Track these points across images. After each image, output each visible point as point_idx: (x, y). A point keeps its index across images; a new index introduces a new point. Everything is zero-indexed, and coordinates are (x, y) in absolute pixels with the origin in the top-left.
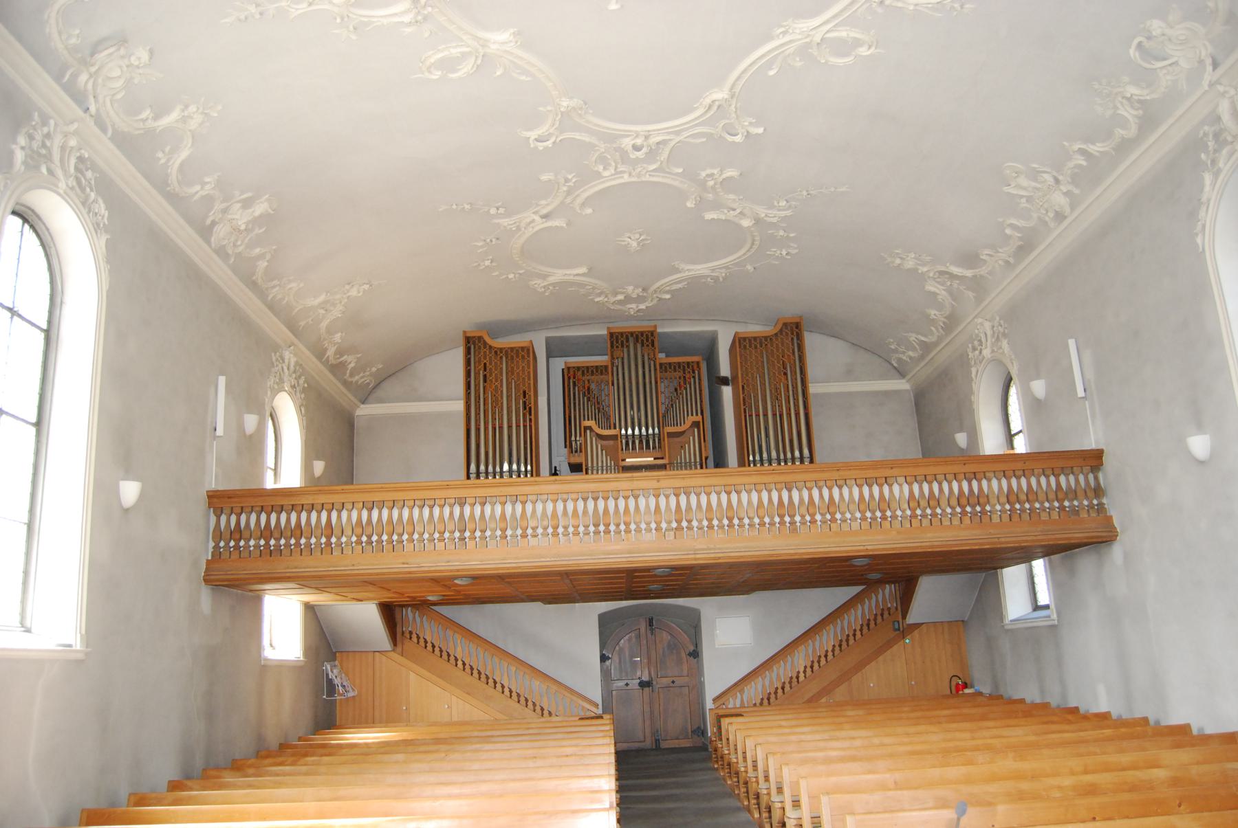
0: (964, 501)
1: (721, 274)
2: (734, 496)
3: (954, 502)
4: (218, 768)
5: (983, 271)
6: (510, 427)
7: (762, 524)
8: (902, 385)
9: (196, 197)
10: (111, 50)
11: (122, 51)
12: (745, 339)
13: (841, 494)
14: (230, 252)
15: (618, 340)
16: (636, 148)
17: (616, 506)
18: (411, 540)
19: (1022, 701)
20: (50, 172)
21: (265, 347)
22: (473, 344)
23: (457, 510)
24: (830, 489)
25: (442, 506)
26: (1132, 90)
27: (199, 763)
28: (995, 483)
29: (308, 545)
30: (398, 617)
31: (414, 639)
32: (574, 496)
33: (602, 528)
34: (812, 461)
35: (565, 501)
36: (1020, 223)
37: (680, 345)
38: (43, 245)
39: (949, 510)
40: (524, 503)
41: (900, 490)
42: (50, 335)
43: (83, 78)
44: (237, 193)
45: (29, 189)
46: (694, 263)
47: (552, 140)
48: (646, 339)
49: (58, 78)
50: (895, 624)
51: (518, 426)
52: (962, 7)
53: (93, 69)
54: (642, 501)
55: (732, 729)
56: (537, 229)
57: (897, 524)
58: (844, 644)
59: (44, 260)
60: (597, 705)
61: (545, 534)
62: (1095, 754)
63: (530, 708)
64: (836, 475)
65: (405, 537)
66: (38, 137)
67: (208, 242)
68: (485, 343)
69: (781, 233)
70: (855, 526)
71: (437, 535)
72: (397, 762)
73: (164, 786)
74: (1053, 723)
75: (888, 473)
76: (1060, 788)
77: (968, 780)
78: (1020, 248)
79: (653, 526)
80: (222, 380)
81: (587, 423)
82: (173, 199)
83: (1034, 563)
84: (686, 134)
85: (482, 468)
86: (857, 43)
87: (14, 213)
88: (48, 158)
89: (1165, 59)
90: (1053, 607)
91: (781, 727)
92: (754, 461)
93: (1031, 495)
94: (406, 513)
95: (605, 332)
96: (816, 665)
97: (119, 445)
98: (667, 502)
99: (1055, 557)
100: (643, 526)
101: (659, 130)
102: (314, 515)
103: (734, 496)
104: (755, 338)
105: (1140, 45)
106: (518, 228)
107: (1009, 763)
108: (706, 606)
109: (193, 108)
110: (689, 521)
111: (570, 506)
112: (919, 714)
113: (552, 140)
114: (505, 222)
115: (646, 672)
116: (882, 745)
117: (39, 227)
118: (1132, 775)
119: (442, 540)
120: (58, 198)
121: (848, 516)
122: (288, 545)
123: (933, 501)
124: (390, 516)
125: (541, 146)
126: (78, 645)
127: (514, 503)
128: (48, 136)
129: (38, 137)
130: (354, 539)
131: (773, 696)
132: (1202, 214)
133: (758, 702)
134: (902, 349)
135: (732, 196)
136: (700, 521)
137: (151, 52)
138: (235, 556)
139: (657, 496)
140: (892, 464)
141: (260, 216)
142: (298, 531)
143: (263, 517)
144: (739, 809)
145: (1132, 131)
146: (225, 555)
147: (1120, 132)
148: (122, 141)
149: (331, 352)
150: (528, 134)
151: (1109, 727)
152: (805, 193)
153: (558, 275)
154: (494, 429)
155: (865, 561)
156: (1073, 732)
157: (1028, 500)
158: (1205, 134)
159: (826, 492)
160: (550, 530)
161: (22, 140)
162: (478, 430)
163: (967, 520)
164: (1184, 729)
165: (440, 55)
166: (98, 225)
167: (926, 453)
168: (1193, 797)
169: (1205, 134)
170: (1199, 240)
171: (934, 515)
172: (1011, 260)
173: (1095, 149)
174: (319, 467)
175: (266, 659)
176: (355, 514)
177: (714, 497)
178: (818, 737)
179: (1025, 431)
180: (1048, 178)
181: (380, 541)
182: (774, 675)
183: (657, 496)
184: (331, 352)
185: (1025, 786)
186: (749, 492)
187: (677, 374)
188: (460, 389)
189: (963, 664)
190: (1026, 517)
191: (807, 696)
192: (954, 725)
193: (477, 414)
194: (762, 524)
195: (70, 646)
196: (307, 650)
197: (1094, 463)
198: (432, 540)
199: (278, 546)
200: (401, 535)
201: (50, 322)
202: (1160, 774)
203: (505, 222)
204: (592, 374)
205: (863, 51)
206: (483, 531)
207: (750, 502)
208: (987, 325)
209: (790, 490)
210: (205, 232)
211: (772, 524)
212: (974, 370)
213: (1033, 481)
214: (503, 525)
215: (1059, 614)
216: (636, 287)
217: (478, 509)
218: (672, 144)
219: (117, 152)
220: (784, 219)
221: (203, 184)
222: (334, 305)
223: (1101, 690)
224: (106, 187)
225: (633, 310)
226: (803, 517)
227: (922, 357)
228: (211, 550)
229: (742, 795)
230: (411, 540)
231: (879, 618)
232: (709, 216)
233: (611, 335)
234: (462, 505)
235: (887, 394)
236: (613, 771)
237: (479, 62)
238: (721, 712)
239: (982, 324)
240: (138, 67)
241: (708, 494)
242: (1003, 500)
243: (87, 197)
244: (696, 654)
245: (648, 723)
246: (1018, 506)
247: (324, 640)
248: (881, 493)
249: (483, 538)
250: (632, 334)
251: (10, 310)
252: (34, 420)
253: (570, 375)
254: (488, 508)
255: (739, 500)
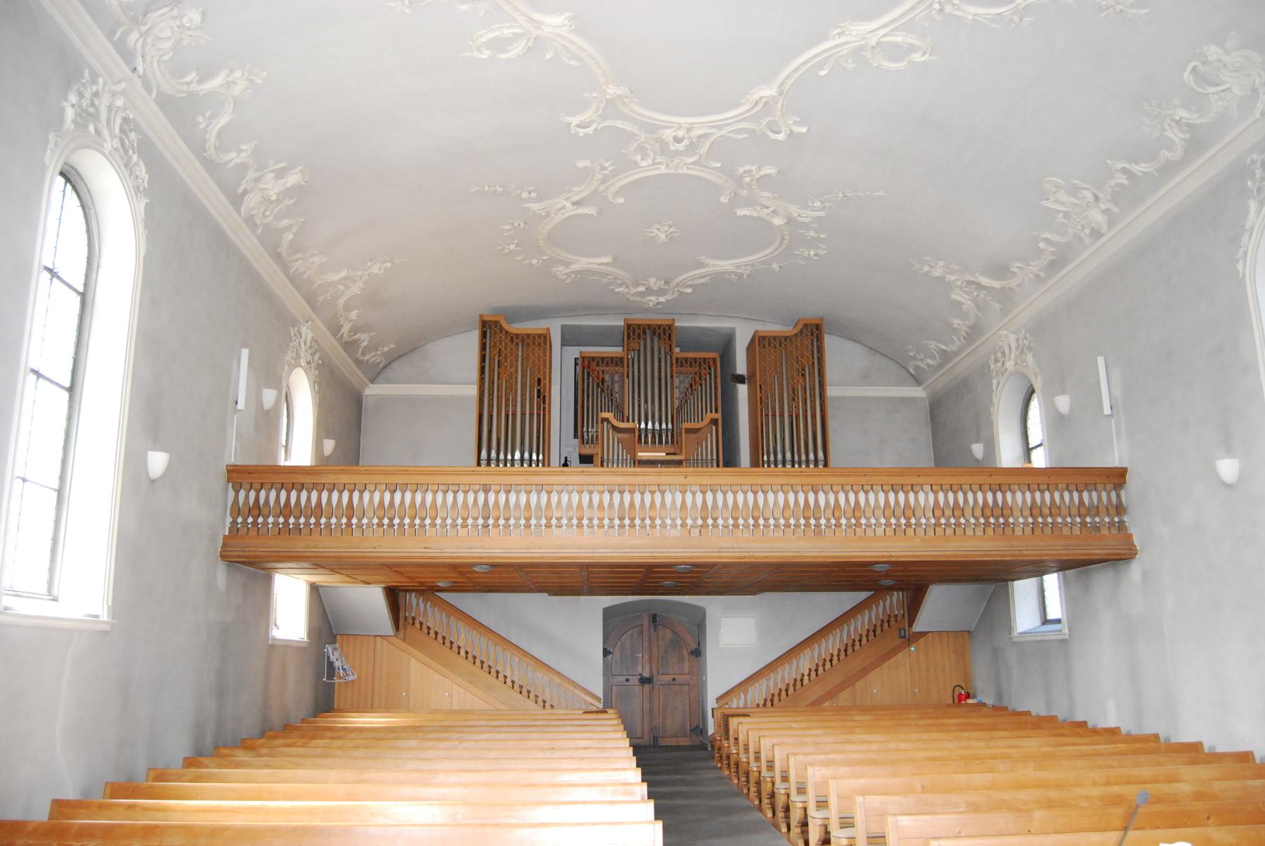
0: (988, 512)
1: (746, 271)
2: (761, 496)
3: (978, 513)
4: (225, 746)
5: (1012, 283)
6: (523, 414)
7: (787, 525)
8: (918, 392)
9: (231, 165)
10: (165, 10)
11: (175, 12)
12: (764, 338)
13: (867, 499)
14: (258, 222)
15: (634, 332)
16: (677, 140)
17: (642, 500)
18: (433, 525)
19: (1027, 713)
20: (97, 131)
21: (284, 321)
22: (489, 329)
23: (481, 496)
24: (856, 493)
25: (466, 492)
26: (1181, 113)
27: (209, 740)
28: (1019, 495)
29: (328, 525)
30: (401, 602)
31: (417, 625)
32: (600, 488)
33: (627, 522)
34: (826, 465)
35: (591, 493)
36: (1055, 238)
37: (698, 340)
38: (83, 206)
39: (973, 521)
40: (549, 493)
41: (925, 498)
42: (85, 299)
43: (134, 36)
44: (271, 162)
45: (76, 149)
46: (719, 258)
47: (593, 127)
48: (664, 332)
49: (110, 35)
50: (900, 632)
51: (531, 414)
52: (1021, 19)
53: (144, 29)
54: (668, 497)
55: (743, 730)
56: (566, 215)
57: (920, 532)
58: (850, 649)
59: (83, 221)
60: (598, 699)
61: (570, 525)
62: (1113, 767)
63: (534, 704)
64: (863, 480)
65: (428, 521)
66: (88, 94)
67: (239, 213)
68: (501, 329)
69: (812, 233)
70: (880, 531)
71: (460, 521)
72: (412, 749)
73: (179, 762)
74: (1063, 735)
75: (915, 480)
76: (1087, 797)
77: (993, 786)
78: (1052, 263)
79: (679, 522)
80: (245, 353)
81: (605, 415)
82: (211, 166)
83: (1046, 577)
84: (729, 129)
85: (493, 454)
86: (912, 49)
87: (62, 174)
88: (96, 117)
89: (1218, 85)
90: (1064, 621)
91: (790, 728)
92: (769, 462)
93: (1054, 509)
94: (429, 497)
95: (622, 323)
96: (821, 669)
97: (150, 416)
98: (694, 499)
99: (1070, 572)
100: (668, 521)
101: (701, 124)
102: (335, 495)
103: (761, 496)
104: (775, 338)
105: (1194, 69)
106: (548, 214)
107: (1028, 773)
108: (712, 605)
109: (238, 74)
110: (715, 519)
111: (596, 498)
112: (928, 722)
113: (593, 127)
114: (536, 207)
115: (647, 669)
116: (898, 750)
117: (81, 187)
118: (1154, 788)
119: (464, 526)
120: (103, 159)
121: (873, 521)
122: (307, 524)
123: (957, 510)
124: (413, 501)
125: (582, 132)
126: (104, 617)
127: (539, 492)
128: (96, 94)
129: (88, 94)
130: (375, 521)
131: (776, 698)
132: (1245, 239)
133: (762, 703)
134: (921, 356)
135: (766, 194)
136: (725, 520)
137: (203, 14)
138: (253, 533)
139: (683, 492)
140: (918, 472)
141: (293, 187)
142: (318, 510)
143: (283, 494)
144: (749, 809)
145: (1178, 153)
146: (243, 532)
147: (1165, 154)
148: (167, 103)
149: (346, 329)
150: (569, 119)
151: (1120, 742)
152: (841, 195)
153: (582, 263)
154: (507, 416)
155: (886, 567)
156: (1089, 744)
157: (1051, 515)
158: (1253, 162)
159: (852, 496)
160: (575, 521)
161: (73, 98)
162: (491, 416)
163: (990, 531)
164: (1195, 747)
165: (491, 35)
166: (138, 188)
167: (937, 465)
168: (1227, 814)
169: (1253, 162)
170: (1240, 266)
171: (958, 524)
172: (1042, 274)
173: (1138, 169)
174: (329, 446)
175: (274, 639)
176: (377, 496)
177: (740, 496)
178: (831, 739)
179: (1046, 443)
180: (1088, 195)
181: (401, 525)
182: (779, 676)
183: (683, 492)
184: (346, 329)
185: (1054, 794)
186: (775, 493)
187: (693, 370)
188: (474, 373)
189: (967, 675)
190: (1048, 531)
191: (810, 700)
192: (966, 734)
193: (491, 400)
194: (787, 525)
195: (97, 616)
196: (311, 631)
197: (1117, 481)
198: (454, 526)
199: (297, 524)
200: (423, 519)
201: (86, 285)
202: (1184, 788)
203: (536, 207)
204: (607, 365)
205: (917, 57)
206: (507, 519)
207: (776, 502)
208: (1012, 337)
209: (816, 493)
210: (237, 200)
211: (797, 525)
212: (995, 382)
213: (1057, 495)
214: (527, 515)
215: (1070, 629)
216: (658, 279)
217: (502, 497)
218: (714, 137)
219: (160, 114)
220: (816, 219)
221: (239, 151)
222: (354, 281)
223: (1111, 706)
224: (147, 150)
225: (652, 302)
226: (828, 520)
227: (941, 366)
228: (228, 525)
229: (752, 794)
230: (433, 525)
231: (886, 625)
232: (741, 212)
233: (629, 326)
234: (486, 491)
235: (903, 400)
236: (633, 761)
237: (530, 44)
238: (728, 712)
239: (1006, 336)
240: (189, 29)
241: (735, 493)
242: (1027, 512)
243: (130, 159)
244: (698, 653)
245: (646, 719)
246: (1040, 520)
247: (327, 622)
248: (907, 500)
249: (507, 526)
250: (649, 326)
251: (50, 271)
252: (67, 385)
253: (586, 366)
254: (513, 497)
255: (766, 500)
